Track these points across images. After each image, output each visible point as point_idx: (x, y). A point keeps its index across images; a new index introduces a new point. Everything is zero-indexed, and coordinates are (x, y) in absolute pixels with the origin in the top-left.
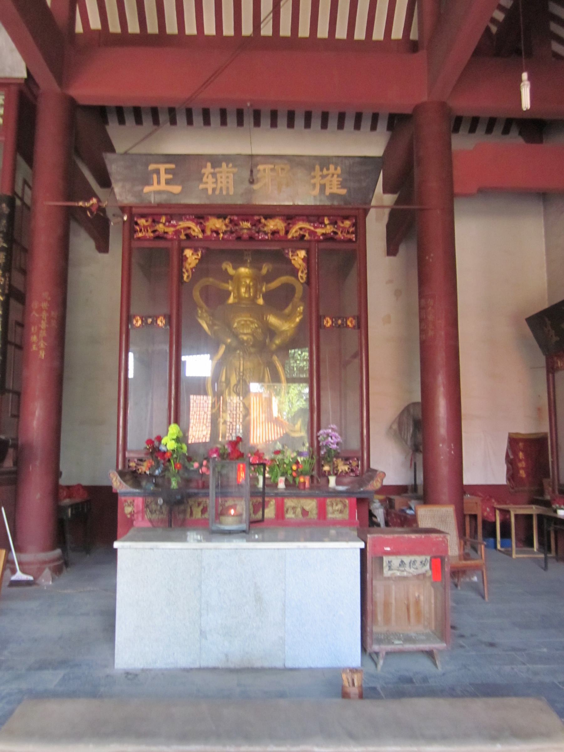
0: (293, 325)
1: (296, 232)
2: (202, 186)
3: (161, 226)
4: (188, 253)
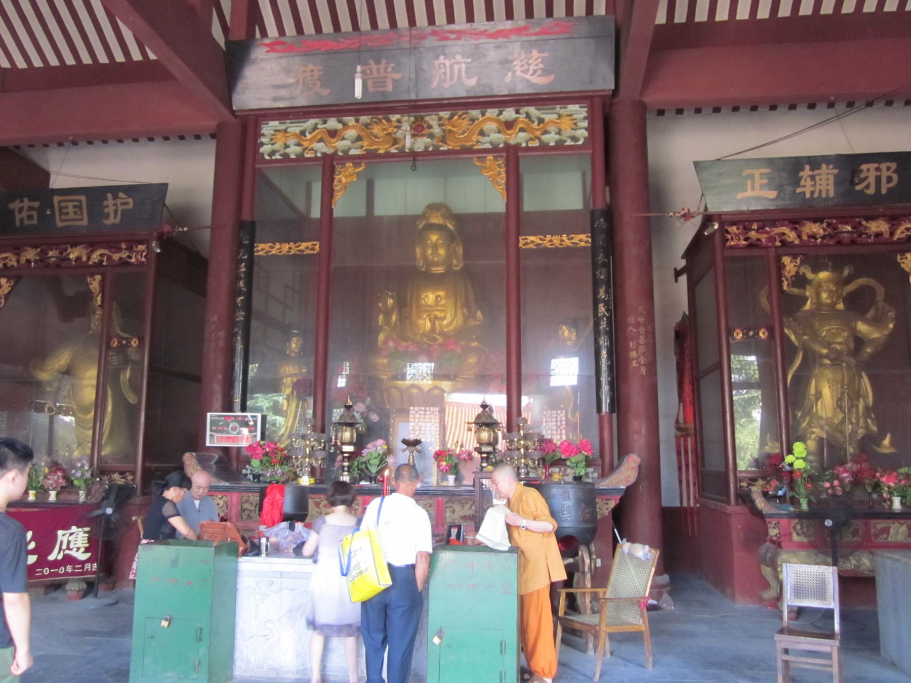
0: (886, 332)
1: (902, 232)
2: (799, 190)
3: (753, 233)
4: (786, 260)
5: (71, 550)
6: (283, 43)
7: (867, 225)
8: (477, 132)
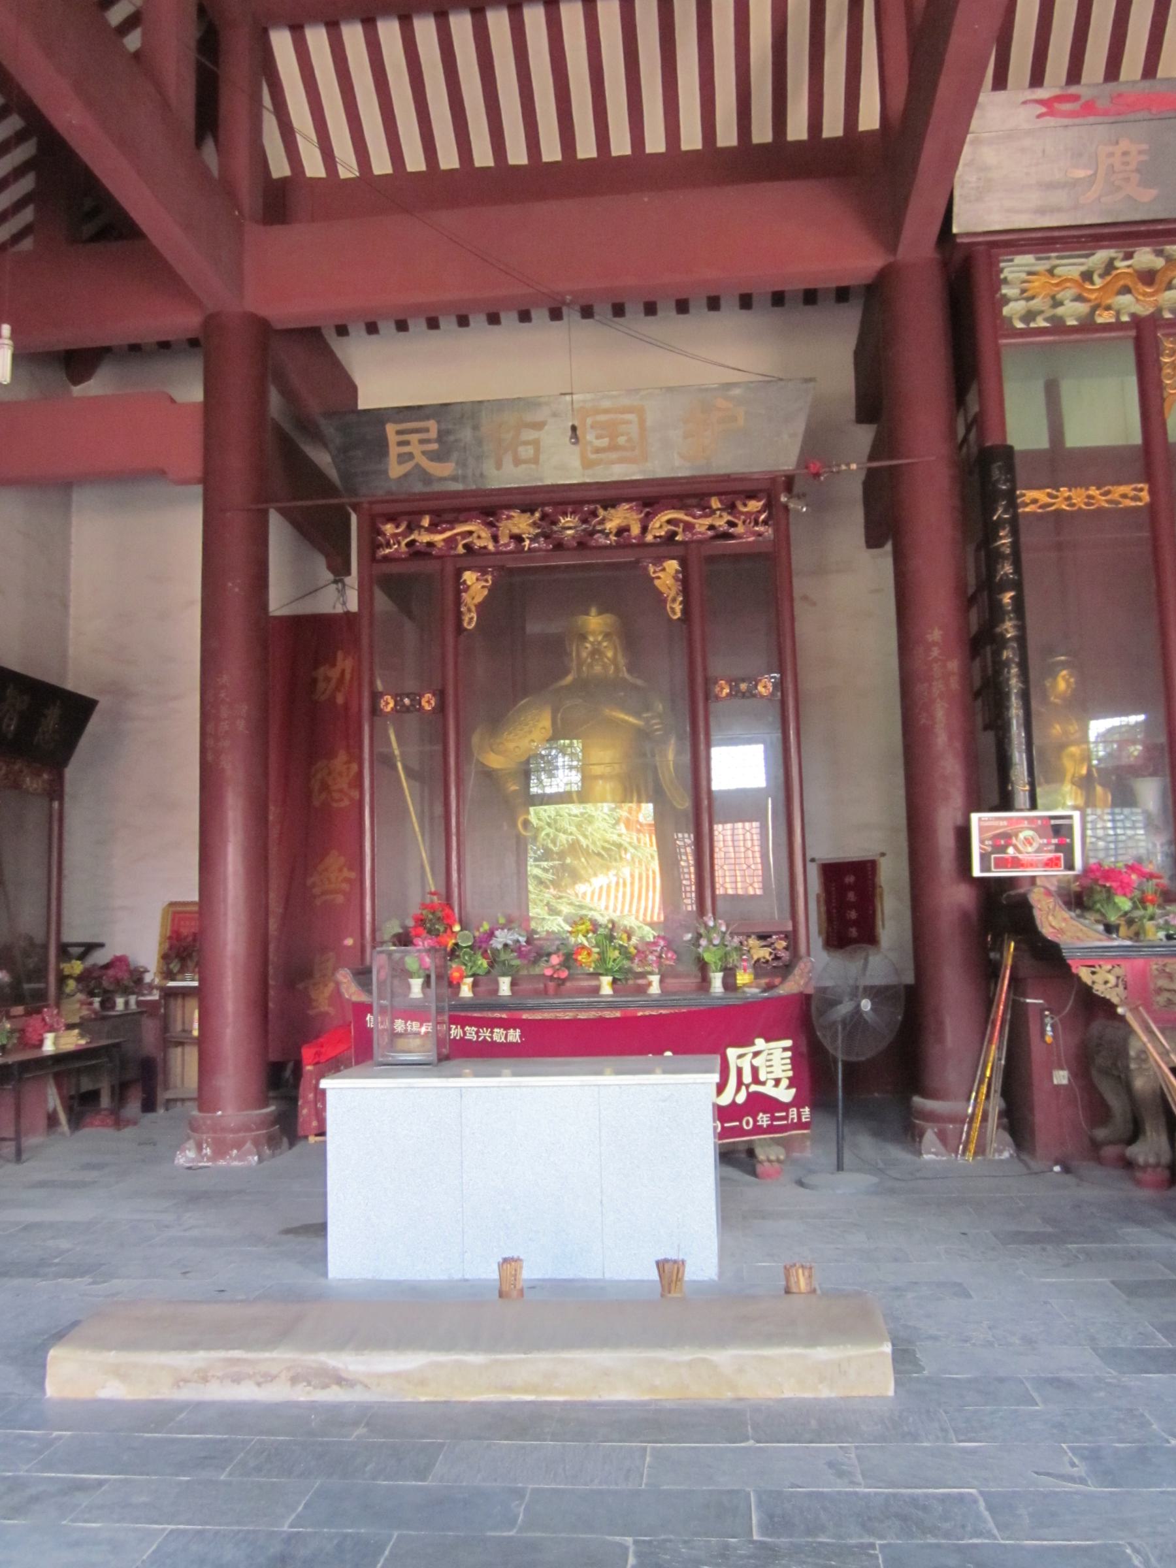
4: (469, 577)
5: (763, 1083)
6: (1075, 98)
7: (601, 517)
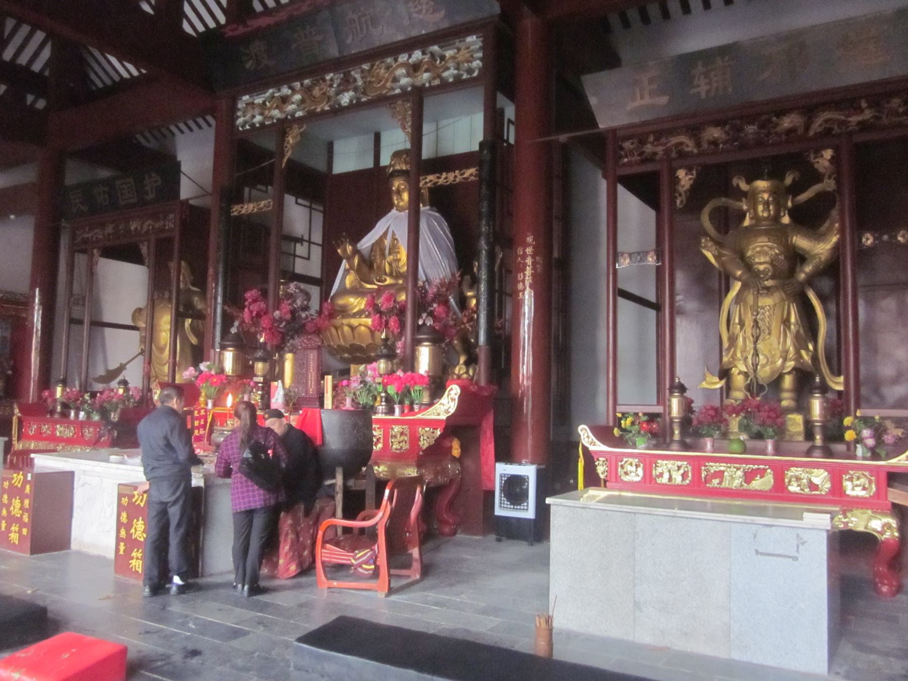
2: (693, 91)
3: (649, 146)
4: (681, 173)
8: (390, 80)
